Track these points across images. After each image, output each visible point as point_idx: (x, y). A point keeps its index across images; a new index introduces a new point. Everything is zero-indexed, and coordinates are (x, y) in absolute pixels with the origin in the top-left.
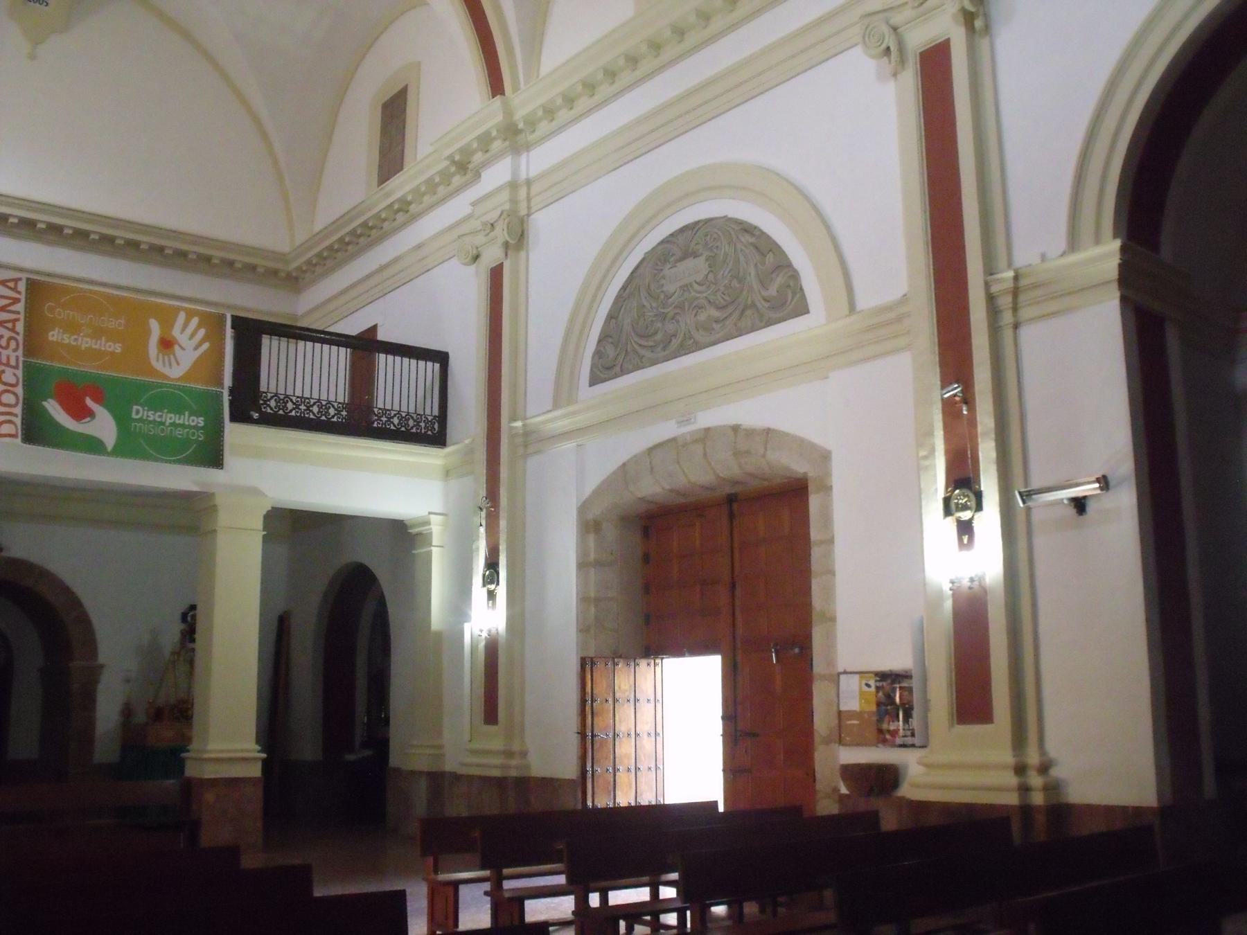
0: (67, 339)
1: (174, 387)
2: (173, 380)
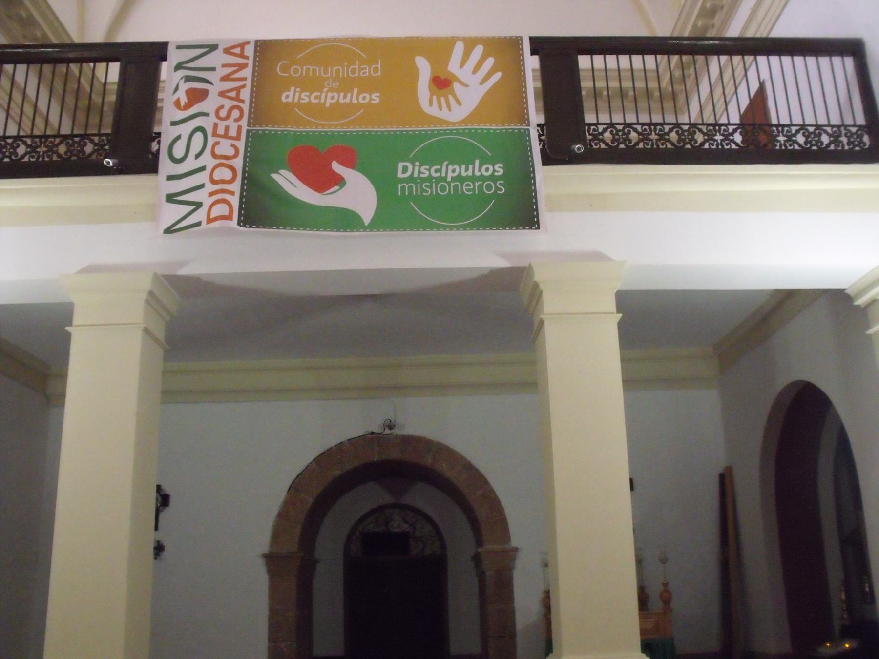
1: (464, 133)
2: (454, 124)
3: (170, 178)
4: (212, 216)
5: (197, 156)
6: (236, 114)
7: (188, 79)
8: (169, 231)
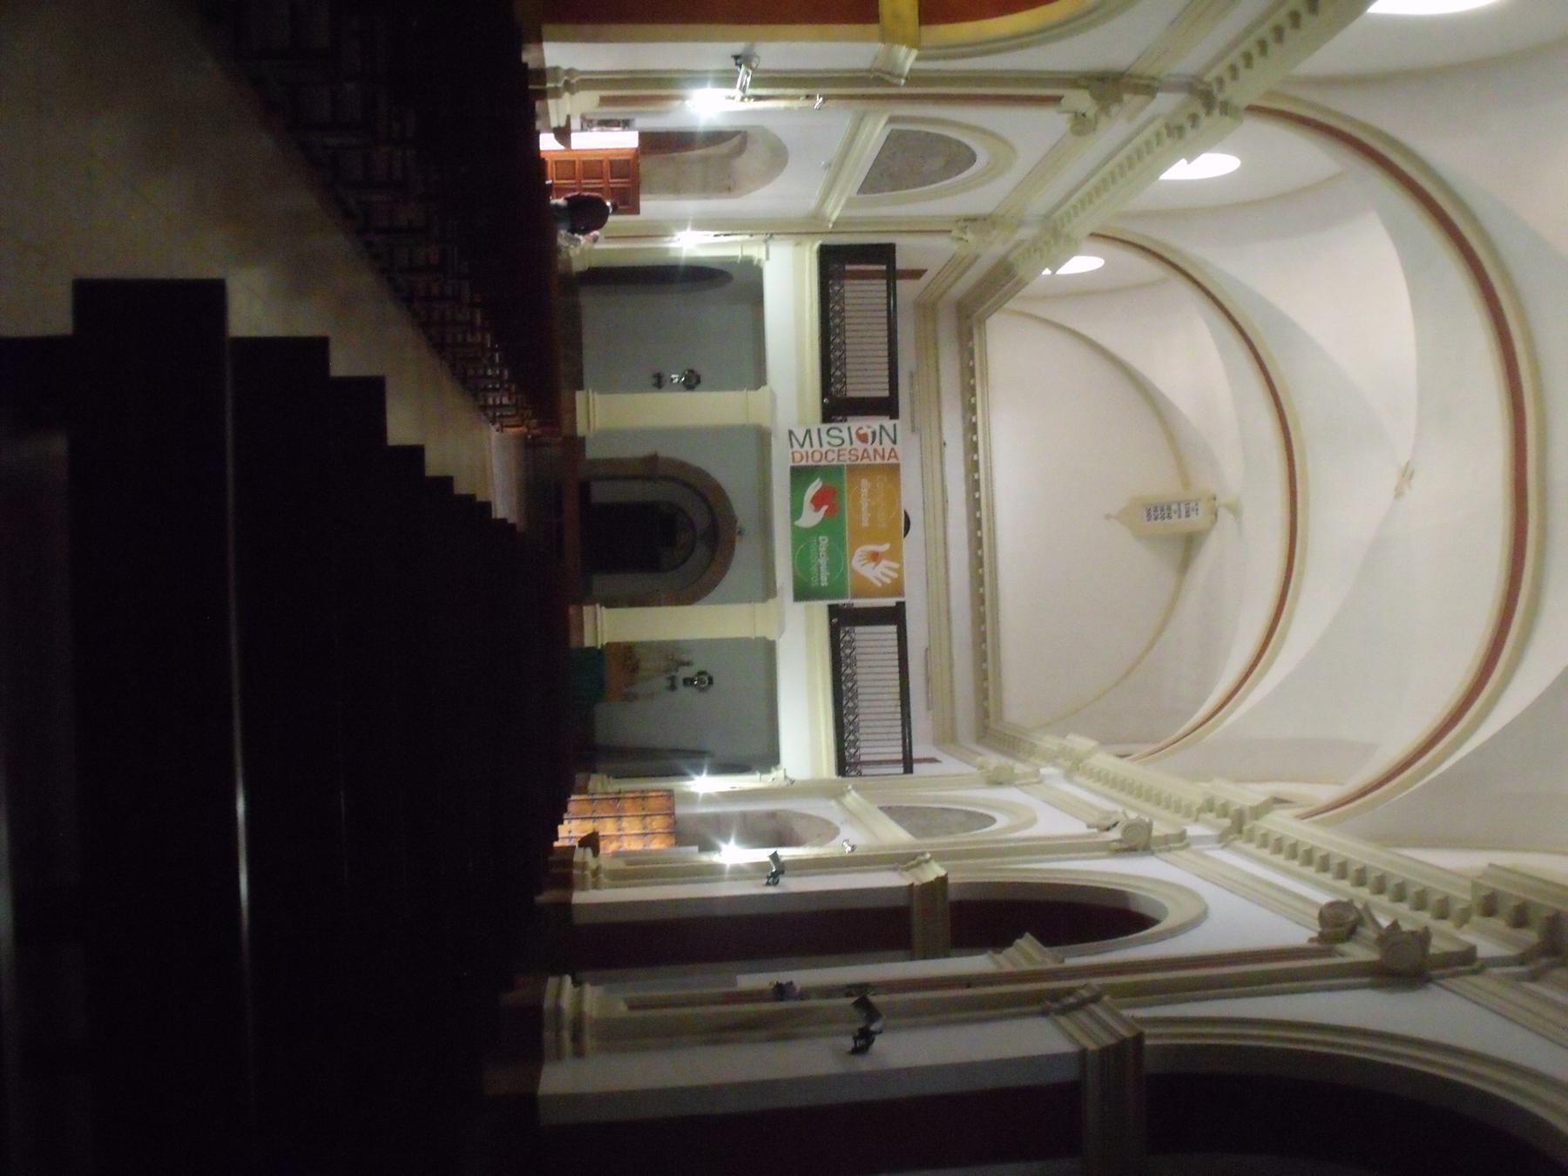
0: (864, 491)
7: (874, 433)
8: (791, 433)
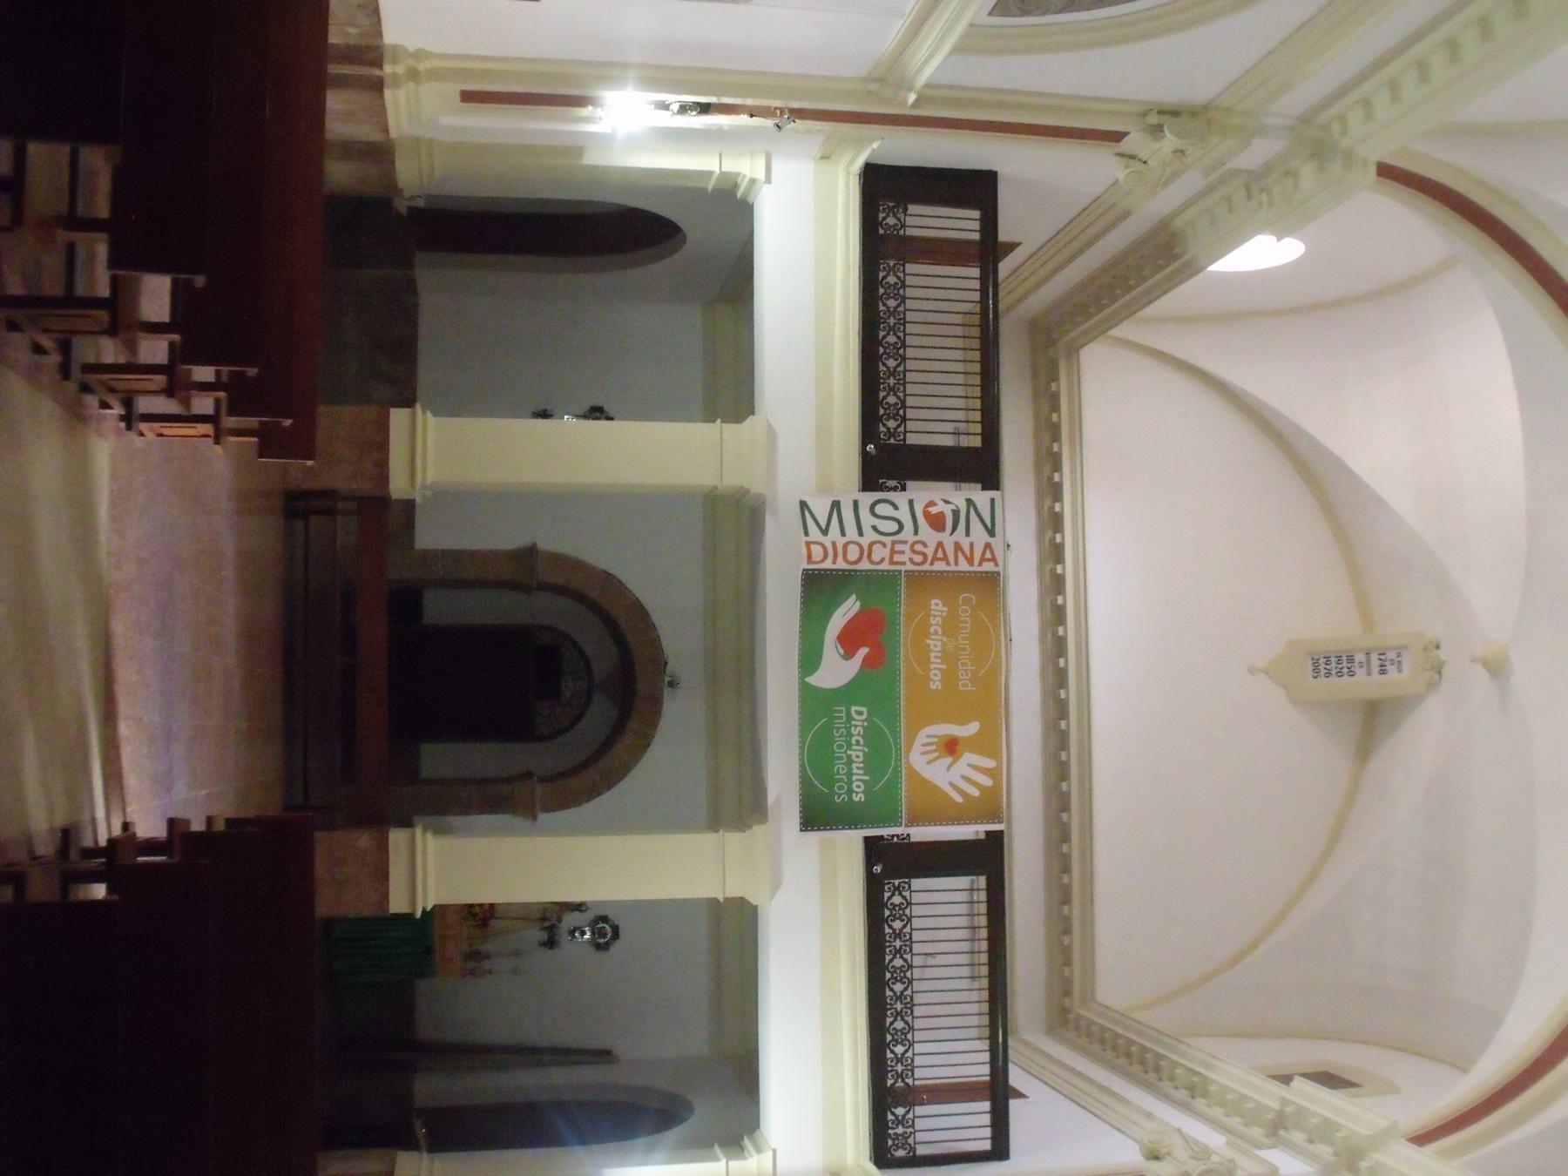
0: (936, 623)
3: (856, 504)
4: (813, 547)
5: (874, 528)
6: (918, 558)
7: (956, 513)
8: (803, 505)
